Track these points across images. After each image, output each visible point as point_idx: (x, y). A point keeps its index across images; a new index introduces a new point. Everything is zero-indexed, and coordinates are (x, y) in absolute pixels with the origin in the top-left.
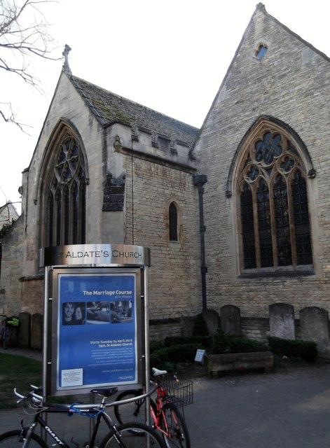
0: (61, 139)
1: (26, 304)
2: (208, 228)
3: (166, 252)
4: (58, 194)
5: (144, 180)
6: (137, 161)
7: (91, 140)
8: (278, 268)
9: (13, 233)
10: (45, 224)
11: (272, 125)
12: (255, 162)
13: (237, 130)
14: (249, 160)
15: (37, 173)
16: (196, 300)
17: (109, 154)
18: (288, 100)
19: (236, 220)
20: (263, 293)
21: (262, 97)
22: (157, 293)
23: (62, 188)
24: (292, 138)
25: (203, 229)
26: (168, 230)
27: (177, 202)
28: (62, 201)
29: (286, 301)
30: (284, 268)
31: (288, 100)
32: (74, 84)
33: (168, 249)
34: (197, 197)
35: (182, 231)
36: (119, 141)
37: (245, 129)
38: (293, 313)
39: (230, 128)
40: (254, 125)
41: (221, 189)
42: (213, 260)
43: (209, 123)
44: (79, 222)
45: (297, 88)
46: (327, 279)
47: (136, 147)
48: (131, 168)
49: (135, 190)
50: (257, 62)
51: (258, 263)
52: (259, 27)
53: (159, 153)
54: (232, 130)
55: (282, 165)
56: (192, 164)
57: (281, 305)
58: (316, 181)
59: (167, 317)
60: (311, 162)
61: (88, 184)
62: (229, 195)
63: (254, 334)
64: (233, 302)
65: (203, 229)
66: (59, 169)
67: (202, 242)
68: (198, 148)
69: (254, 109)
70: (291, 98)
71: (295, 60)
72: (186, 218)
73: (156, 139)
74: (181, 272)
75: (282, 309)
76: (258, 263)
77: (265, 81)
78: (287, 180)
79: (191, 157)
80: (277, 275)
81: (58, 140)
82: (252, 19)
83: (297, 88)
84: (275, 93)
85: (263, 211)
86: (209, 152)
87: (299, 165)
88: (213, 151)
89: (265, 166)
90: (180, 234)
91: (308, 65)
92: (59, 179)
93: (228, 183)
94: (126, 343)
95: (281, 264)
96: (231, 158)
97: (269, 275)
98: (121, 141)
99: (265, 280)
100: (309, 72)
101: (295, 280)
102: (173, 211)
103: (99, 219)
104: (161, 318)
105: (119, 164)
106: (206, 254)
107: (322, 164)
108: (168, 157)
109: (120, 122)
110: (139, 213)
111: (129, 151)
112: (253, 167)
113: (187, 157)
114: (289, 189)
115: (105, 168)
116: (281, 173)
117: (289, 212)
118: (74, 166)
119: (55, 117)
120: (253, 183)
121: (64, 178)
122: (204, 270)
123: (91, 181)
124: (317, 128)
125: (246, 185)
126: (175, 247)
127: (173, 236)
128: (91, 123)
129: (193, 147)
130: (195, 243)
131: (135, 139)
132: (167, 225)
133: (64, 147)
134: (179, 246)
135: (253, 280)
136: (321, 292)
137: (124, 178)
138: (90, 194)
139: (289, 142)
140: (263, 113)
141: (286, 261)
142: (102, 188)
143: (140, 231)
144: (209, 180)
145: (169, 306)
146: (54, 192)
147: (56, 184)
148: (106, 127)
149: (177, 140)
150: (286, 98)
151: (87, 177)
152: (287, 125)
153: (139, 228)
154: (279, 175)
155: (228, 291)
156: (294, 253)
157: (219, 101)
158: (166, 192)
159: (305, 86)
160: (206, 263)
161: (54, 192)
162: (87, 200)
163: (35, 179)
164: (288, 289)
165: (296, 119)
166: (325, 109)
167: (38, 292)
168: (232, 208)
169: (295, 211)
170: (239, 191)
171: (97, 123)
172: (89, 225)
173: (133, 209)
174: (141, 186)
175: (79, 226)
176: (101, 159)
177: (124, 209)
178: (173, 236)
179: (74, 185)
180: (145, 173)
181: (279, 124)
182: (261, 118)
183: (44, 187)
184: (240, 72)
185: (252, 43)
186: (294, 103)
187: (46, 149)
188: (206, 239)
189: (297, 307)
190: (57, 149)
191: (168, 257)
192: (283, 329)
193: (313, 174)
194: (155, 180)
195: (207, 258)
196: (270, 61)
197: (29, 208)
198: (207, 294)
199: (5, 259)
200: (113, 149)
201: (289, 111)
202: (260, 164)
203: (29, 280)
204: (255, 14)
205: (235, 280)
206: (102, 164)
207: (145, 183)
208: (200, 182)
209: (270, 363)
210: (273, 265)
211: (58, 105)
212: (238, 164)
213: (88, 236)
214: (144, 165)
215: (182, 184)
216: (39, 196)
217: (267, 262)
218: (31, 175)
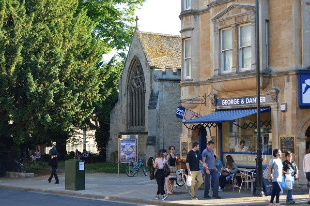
28: (137, 95)
92: (135, 84)
94: (290, 133)
105: (157, 86)
115: (151, 87)
121: (138, 85)
146: (133, 90)
161: (133, 90)
214: (168, 84)
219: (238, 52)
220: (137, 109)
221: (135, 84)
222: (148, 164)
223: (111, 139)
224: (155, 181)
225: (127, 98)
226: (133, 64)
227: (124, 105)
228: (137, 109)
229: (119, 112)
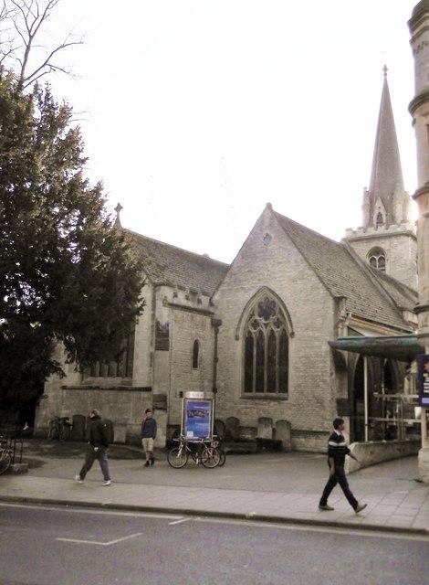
1: (68, 408)
2: (220, 360)
6: (176, 311)
12: (257, 317)
14: (253, 315)
24: (282, 307)
25: (216, 360)
29: (269, 416)
37: (252, 293)
38: (272, 423)
39: (242, 288)
41: (232, 331)
51: (254, 389)
52: (267, 221)
53: (190, 304)
56: (211, 310)
57: (266, 418)
60: (292, 327)
62: (237, 338)
63: (248, 436)
64: (234, 415)
65: (216, 360)
67: (215, 368)
68: (216, 297)
69: (259, 280)
75: (265, 421)
76: (254, 389)
78: (277, 335)
79: (211, 304)
80: (265, 398)
84: (274, 273)
85: (261, 352)
97: (260, 398)
99: (257, 401)
102: (196, 344)
108: (196, 306)
111: (173, 306)
112: (255, 321)
114: (278, 341)
115: (153, 315)
117: (277, 357)
125: (250, 333)
126: (196, 373)
130: (209, 370)
131: (175, 296)
141: (271, 389)
154: (272, 330)
155: (231, 407)
156: (277, 385)
164: (272, 409)
165: (286, 295)
168: (238, 349)
169: (281, 357)
170: (244, 336)
172: (137, 355)
178: (195, 365)
184: (252, 249)
188: (218, 368)
189: (275, 420)
192: (265, 433)
193: (293, 334)
195: (217, 382)
203: (73, 388)
208: (216, 324)
209: (254, 449)
212: (246, 317)
217: (260, 389)
223: (47, 397)
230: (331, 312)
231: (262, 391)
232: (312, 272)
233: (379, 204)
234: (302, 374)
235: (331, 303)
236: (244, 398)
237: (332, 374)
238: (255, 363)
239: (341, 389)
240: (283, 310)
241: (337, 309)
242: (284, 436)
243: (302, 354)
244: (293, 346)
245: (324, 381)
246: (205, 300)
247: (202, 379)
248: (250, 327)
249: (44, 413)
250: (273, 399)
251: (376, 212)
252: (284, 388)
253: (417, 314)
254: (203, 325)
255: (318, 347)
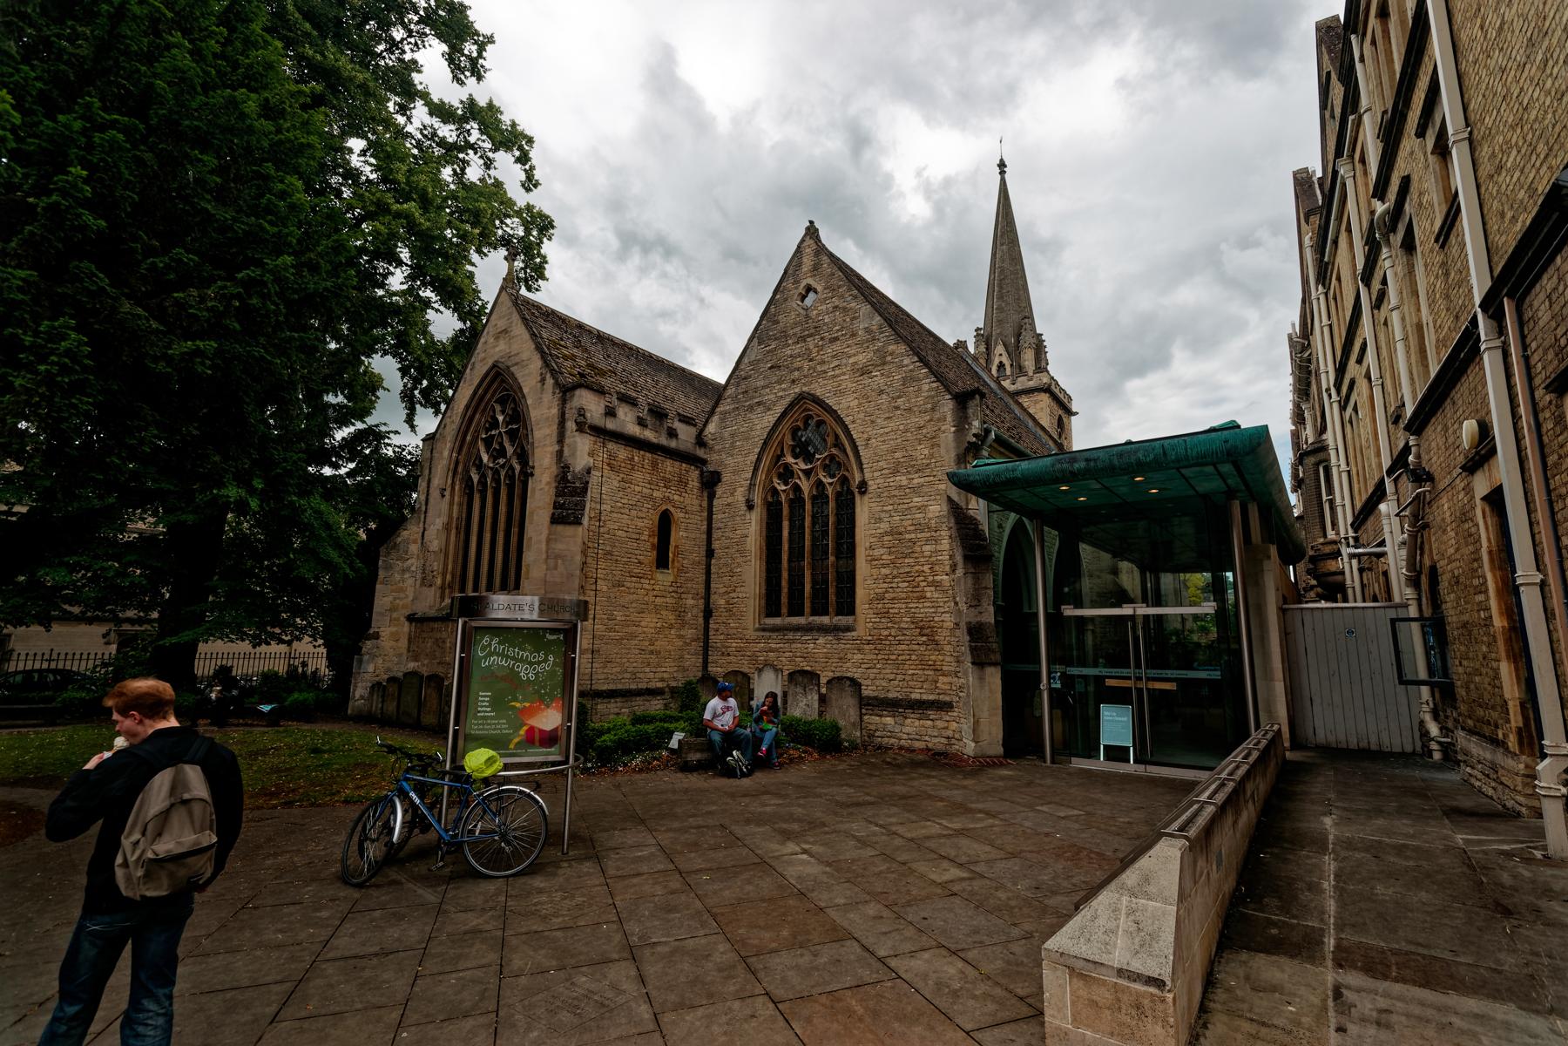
0: (493, 396)
2: (718, 553)
3: (647, 587)
4: (483, 482)
5: (622, 475)
6: (611, 446)
7: (541, 408)
8: (811, 618)
9: (399, 539)
10: (457, 528)
11: (815, 409)
12: (790, 460)
13: (769, 409)
14: (782, 455)
15: (449, 445)
16: (693, 662)
17: (568, 433)
18: (838, 376)
19: (758, 543)
20: (787, 654)
21: (806, 365)
22: (629, 649)
23: (490, 473)
26: (655, 552)
27: (672, 509)
30: (818, 620)
31: (838, 376)
32: (520, 312)
33: (653, 582)
34: (705, 504)
35: (676, 554)
36: (584, 416)
37: (779, 409)
39: (759, 404)
40: (791, 405)
41: (740, 496)
42: (722, 602)
43: (752, 356)
44: (515, 530)
45: (851, 360)
46: (870, 638)
47: (610, 425)
48: (602, 456)
49: (604, 490)
50: (802, 312)
51: (784, 610)
53: (649, 435)
54: (761, 408)
55: (826, 467)
56: (700, 453)
57: (803, 673)
58: (866, 498)
59: (643, 686)
60: (861, 470)
61: (532, 475)
62: (750, 506)
65: (710, 553)
66: (488, 442)
68: (712, 428)
69: (793, 381)
70: (844, 374)
71: (852, 319)
72: (685, 534)
73: (646, 412)
74: (672, 618)
75: (802, 678)
77: (811, 343)
79: (700, 442)
80: (808, 629)
81: (488, 396)
82: (799, 247)
83: (851, 360)
84: (823, 362)
86: (726, 435)
87: (848, 470)
88: (733, 436)
89: (804, 467)
90: (673, 560)
91: (868, 330)
92: (485, 458)
93: (751, 486)
95: (814, 613)
96: (757, 450)
97: (797, 629)
98: (588, 415)
99: (790, 636)
100: (867, 341)
101: (830, 638)
102: (665, 521)
103: (545, 533)
104: (633, 686)
105: (582, 451)
106: (713, 590)
107: (876, 474)
108: (663, 440)
109: (589, 387)
110: (610, 525)
111: (598, 431)
112: (787, 466)
113: (693, 441)
115: (560, 454)
116: (824, 480)
118: (512, 442)
119: (484, 359)
120: (784, 491)
121: (494, 458)
122: (708, 613)
123: (537, 472)
124: (873, 422)
125: (775, 492)
126: (665, 578)
127: (662, 562)
128: (543, 381)
129: (705, 425)
132: (653, 545)
133: (498, 408)
134: (671, 578)
135: (774, 635)
136: (862, 656)
137: (589, 472)
138: (534, 489)
139: (837, 437)
140: (805, 389)
142: (554, 485)
143: (609, 553)
144: (724, 480)
145: (647, 670)
146: (475, 478)
147: (479, 465)
148: (566, 392)
149: (679, 414)
150: (837, 372)
151: (531, 464)
152: (835, 411)
153: (608, 548)
156: (832, 598)
157: (746, 360)
158: (656, 494)
159: (862, 358)
160: (711, 606)
161: (475, 478)
162: (528, 500)
163: (446, 453)
164: (819, 652)
165: (846, 405)
166: (884, 396)
167: (437, 640)
168: (752, 527)
169: (839, 536)
171: (552, 381)
173: (600, 520)
174: (616, 483)
175: (514, 539)
176: (555, 438)
177: (585, 521)
178: (662, 562)
179: (510, 472)
180: (623, 465)
181: (826, 411)
182: (801, 397)
183: (460, 469)
184: (777, 322)
185: (797, 282)
186: (847, 382)
187: (467, 407)
188: (713, 569)
190: (484, 410)
191: (651, 593)
194: (638, 476)
196: (818, 315)
197: (431, 501)
198: (710, 653)
199: (381, 583)
200: (574, 427)
201: (839, 393)
202: (796, 463)
204: (803, 241)
205: (751, 633)
206: (557, 447)
207: (623, 480)
210: (802, 615)
211: (492, 340)
213: (524, 583)
214: (622, 453)
215: (683, 483)
216: (449, 482)
217: (796, 610)
218: (439, 445)
219: (840, 831)
220: (487, 537)
221: (485, 458)
222: (550, 747)
223: (377, 636)
224: (951, 342)
225: (451, 504)
226: (486, 391)
227: (436, 523)
228: (487, 537)
229: (414, 548)
230: (949, 428)
231: (801, 614)
232: (902, 348)
233: (1000, 349)
234: (884, 571)
235: (947, 406)
236: (764, 630)
237: (954, 568)
238: (785, 557)
239: (975, 600)
240: (842, 436)
241: (962, 421)
242: (844, 713)
243: (884, 526)
244: (864, 511)
245: (936, 585)
246: (686, 434)
247: (678, 590)
248: (776, 480)
249: (371, 668)
250: (824, 630)
251: (996, 361)
252: (847, 606)
253: (1403, 178)
254: (683, 483)
255: (922, 508)
